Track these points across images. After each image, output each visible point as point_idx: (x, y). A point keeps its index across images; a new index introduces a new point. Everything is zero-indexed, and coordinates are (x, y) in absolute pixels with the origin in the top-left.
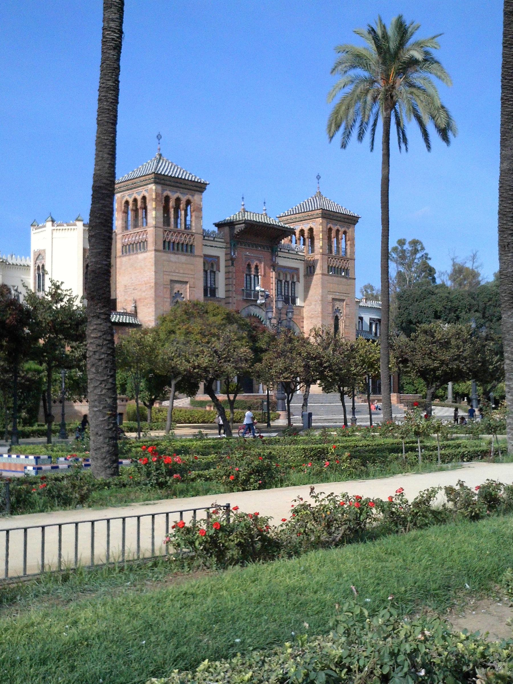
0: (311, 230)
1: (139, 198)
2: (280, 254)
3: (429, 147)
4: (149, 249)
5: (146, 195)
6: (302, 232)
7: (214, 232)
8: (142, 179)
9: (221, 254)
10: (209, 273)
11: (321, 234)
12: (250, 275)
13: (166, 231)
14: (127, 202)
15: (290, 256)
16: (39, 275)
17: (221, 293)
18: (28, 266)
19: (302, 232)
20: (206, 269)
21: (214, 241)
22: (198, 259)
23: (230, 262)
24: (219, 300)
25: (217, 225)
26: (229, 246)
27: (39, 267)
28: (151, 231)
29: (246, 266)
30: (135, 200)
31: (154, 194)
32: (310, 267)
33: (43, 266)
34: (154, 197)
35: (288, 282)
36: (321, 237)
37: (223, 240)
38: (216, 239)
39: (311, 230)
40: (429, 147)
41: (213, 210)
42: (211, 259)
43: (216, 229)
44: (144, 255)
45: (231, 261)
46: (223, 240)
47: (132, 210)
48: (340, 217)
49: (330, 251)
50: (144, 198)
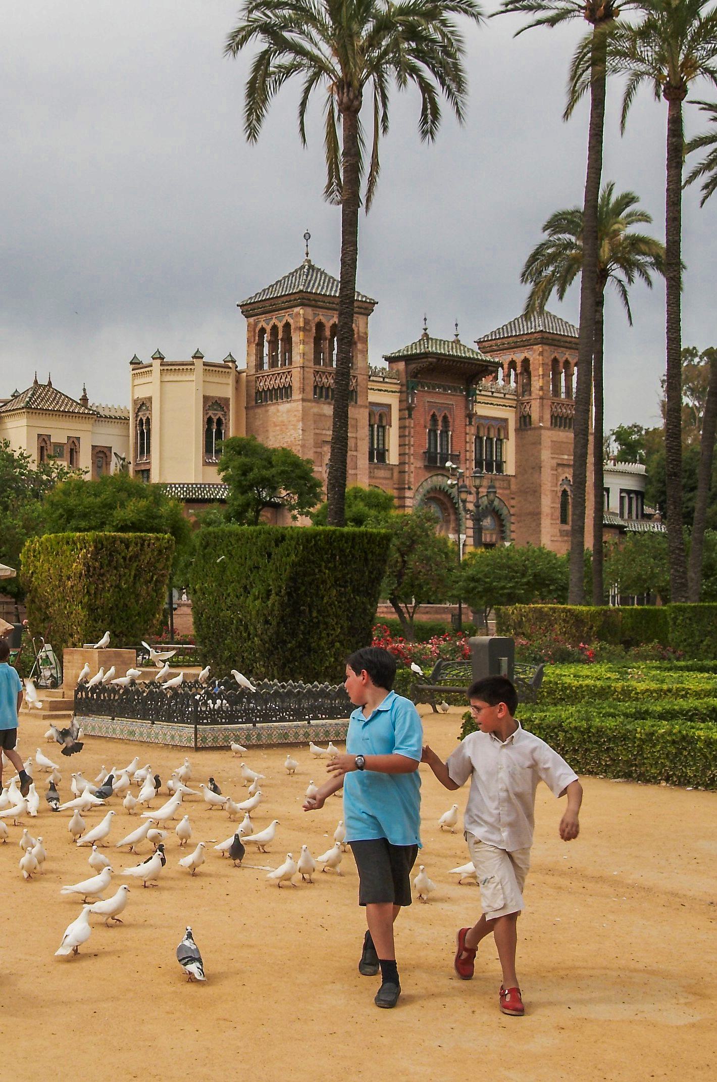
0: (526, 361)
1: (280, 325)
2: (479, 399)
3: (567, 115)
4: (294, 397)
5: (291, 321)
6: (512, 364)
7: (384, 369)
8: (284, 299)
9: (393, 400)
10: (375, 429)
11: (541, 369)
12: (435, 431)
13: (318, 372)
14: (263, 331)
15: (495, 401)
16: (142, 433)
17: (393, 458)
18: (125, 419)
19: (512, 364)
20: (372, 422)
21: (384, 382)
22: (362, 410)
23: (407, 412)
24: (391, 468)
25: (387, 359)
26: (404, 389)
27: (141, 420)
28: (296, 373)
29: (429, 418)
30: (275, 328)
31: (301, 320)
32: (525, 417)
33: (148, 420)
34: (302, 325)
35: (491, 439)
36: (541, 373)
37: (395, 381)
38: (386, 380)
39: (526, 361)
40: (567, 115)
41: (385, 338)
42: (379, 409)
43: (386, 365)
44: (287, 406)
45: (408, 410)
46: (395, 381)
47: (269, 342)
48: (570, 342)
49: (556, 391)
50: (287, 326)
